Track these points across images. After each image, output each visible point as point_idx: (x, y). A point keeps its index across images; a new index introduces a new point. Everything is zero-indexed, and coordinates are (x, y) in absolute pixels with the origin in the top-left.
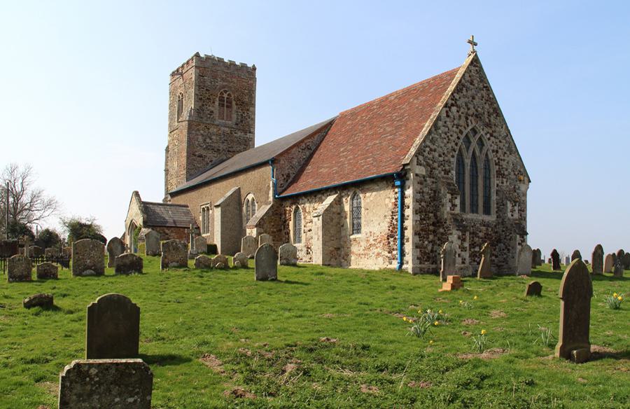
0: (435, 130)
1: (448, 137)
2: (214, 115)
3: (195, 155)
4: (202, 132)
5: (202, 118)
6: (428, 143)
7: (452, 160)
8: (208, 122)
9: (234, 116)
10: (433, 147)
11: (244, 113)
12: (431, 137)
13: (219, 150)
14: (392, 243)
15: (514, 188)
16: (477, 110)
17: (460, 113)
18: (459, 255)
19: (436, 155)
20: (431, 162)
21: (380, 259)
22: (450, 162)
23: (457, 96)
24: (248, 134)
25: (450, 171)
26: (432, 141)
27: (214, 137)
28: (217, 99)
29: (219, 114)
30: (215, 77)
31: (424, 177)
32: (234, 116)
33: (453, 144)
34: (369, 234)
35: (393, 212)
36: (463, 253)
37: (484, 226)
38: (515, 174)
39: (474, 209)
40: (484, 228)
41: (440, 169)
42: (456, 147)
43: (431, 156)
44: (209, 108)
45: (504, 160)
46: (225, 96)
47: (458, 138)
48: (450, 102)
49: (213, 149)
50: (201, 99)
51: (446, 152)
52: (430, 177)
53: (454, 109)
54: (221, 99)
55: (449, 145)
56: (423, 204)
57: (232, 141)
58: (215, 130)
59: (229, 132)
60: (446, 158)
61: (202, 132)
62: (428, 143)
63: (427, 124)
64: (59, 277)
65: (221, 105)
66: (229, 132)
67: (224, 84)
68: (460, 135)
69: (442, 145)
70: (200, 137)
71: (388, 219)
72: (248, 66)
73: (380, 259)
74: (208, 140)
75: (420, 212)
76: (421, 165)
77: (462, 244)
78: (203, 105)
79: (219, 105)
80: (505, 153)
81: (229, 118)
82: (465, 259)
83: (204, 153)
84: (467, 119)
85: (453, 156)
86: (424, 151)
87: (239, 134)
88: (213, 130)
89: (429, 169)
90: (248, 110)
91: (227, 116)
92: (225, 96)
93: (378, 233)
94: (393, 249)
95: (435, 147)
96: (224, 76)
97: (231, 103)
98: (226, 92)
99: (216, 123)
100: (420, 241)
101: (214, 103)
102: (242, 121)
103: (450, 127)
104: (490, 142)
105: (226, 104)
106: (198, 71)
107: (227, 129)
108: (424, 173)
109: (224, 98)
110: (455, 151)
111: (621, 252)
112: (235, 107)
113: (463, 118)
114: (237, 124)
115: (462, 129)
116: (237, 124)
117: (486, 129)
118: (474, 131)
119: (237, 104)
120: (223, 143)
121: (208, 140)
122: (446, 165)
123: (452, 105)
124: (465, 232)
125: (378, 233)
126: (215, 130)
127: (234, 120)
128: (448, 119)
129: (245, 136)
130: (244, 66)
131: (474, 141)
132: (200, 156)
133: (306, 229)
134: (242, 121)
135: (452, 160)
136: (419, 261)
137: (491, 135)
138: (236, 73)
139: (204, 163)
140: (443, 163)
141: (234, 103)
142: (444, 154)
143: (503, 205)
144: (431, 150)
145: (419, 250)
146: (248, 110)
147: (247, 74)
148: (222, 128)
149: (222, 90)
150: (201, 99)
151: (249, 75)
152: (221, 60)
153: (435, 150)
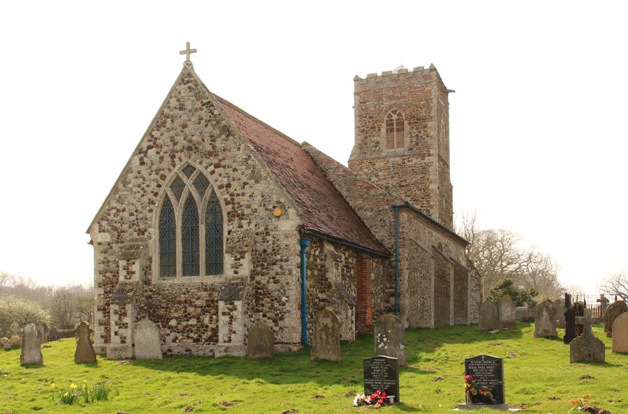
0: (124, 186)
1: (143, 189)
4: (366, 170)
5: (365, 153)
6: (114, 204)
7: (149, 215)
9: (407, 140)
10: (120, 207)
11: (420, 132)
12: (117, 196)
15: (266, 229)
16: (190, 141)
17: (162, 154)
18: (116, 333)
19: (126, 214)
20: (118, 225)
22: (146, 219)
23: (156, 134)
25: (146, 230)
26: (120, 201)
27: (380, 173)
28: (384, 125)
30: (379, 99)
31: (109, 244)
32: (407, 140)
33: (151, 196)
36: (122, 331)
37: (205, 290)
38: (267, 209)
39: (191, 268)
40: (204, 294)
41: (131, 230)
42: (155, 198)
43: (118, 218)
45: (243, 194)
46: (395, 117)
47: (159, 186)
48: (145, 145)
50: (363, 131)
51: (139, 208)
52: (117, 242)
53: (152, 152)
55: (145, 199)
56: (109, 275)
57: (406, 173)
58: (382, 164)
59: (400, 162)
60: (140, 216)
61: (366, 170)
62: (114, 204)
64: (44, 364)
65: (390, 130)
67: (392, 102)
68: (161, 182)
69: (134, 201)
72: (378, 75)
75: (104, 285)
76: (104, 231)
77: (120, 319)
78: (366, 138)
79: (387, 131)
80: (245, 184)
81: (401, 143)
82: (125, 338)
84: (173, 157)
85: (151, 211)
86: (109, 215)
87: (414, 160)
88: (380, 164)
89: (116, 233)
90: (425, 127)
91: (398, 143)
92: (395, 117)
95: (124, 206)
96: (391, 93)
99: (383, 154)
100: (105, 317)
101: (379, 130)
102: (417, 144)
103: (146, 176)
104: (215, 176)
105: (395, 127)
106: (359, 97)
107: (398, 159)
108: (109, 240)
109: (393, 120)
110: (153, 203)
112: (407, 127)
113: (167, 159)
114: (411, 149)
115: (165, 172)
117: (206, 161)
118: (188, 170)
119: (410, 124)
120: (393, 177)
122: (140, 224)
123: (150, 147)
124: (125, 305)
126: (382, 164)
128: (142, 168)
129: (423, 162)
130: (419, 71)
131: (188, 182)
134: (417, 144)
135: (149, 215)
136: (103, 340)
137: (217, 166)
138: (407, 83)
140: (136, 222)
141: (406, 122)
142: (136, 211)
144: (118, 211)
145: (103, 327)
146: (425, 127)
148: (392, 159)
150: (363, 131)
152: (403, 73)
153: (124, 210)
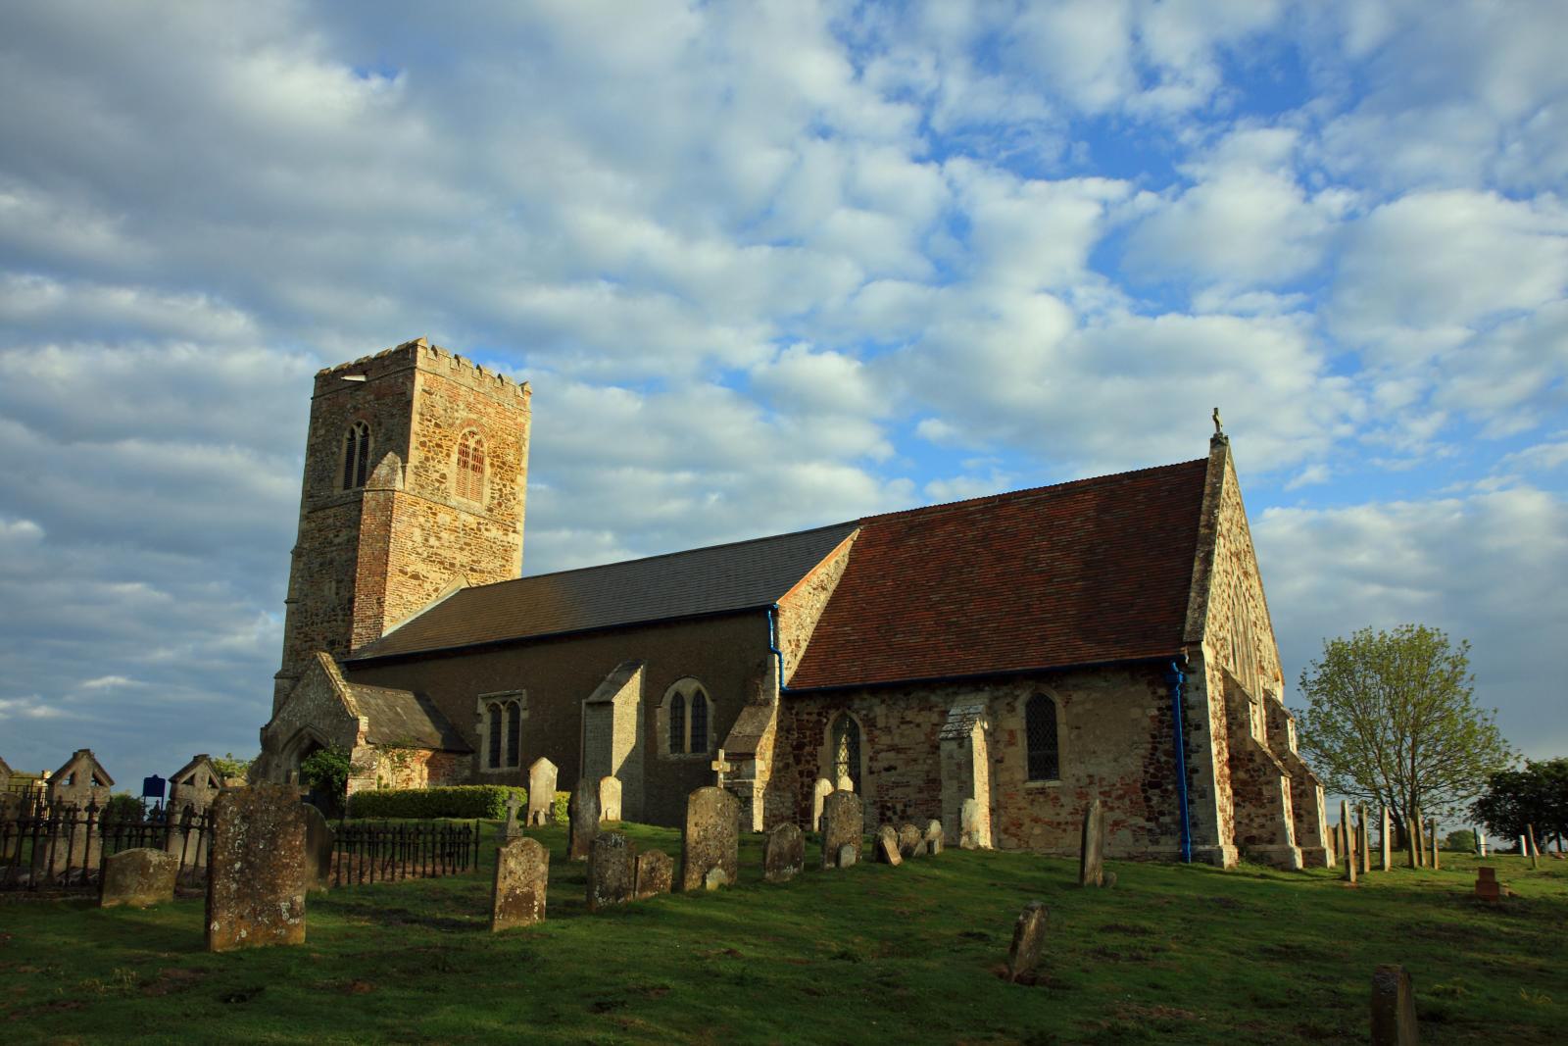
2: (448, 484)
3: (406, 574)
4: (422, 520)
5: (422, 487)
8: (436, 499)
9: (487, 491)
11: (504, 486)
13: (452, 565)
14: (1155, 800)
21: (1125, 834)
24: (511, 535)
27: (444, 535)
28: (456, 448)
29: (458, 483)
32: (487, 491)
34: (1085, 781)
35: (1153, 737)
44: (438, 467)
46: (472, 443)
49: (441, 563)
54: (463, 452)
58: (448, 519)
59: (475, 526)
63: (729, 915)
66: (475, 526)
70: (417, 532)
71: (1144, 749)
73: (1125, 834)
74: (433, 541)
83: (421, 568)
88: (444, 518)
93: (1115, 779)
94: (1162, 814)
97: (481, 461)
98: (473, 433)
101: (448, 455)
102: (500, 504)
111: (155, 776)
112: (488, 471)
116: (490, 510)
119: (492, 465)
120: (462, 549)
121: (433, 541)
125: (1115, 779)
127: (487, 500)
129: (504, 538)
132: (415, 577)
133: (878, 766)
134: (500, 504)
139: (423, 593)
141: (487, 461)
143: (1277, 728)
147: (514, 402)
148: (463, 516)
149: (364, 421)
151: (518, 404)
